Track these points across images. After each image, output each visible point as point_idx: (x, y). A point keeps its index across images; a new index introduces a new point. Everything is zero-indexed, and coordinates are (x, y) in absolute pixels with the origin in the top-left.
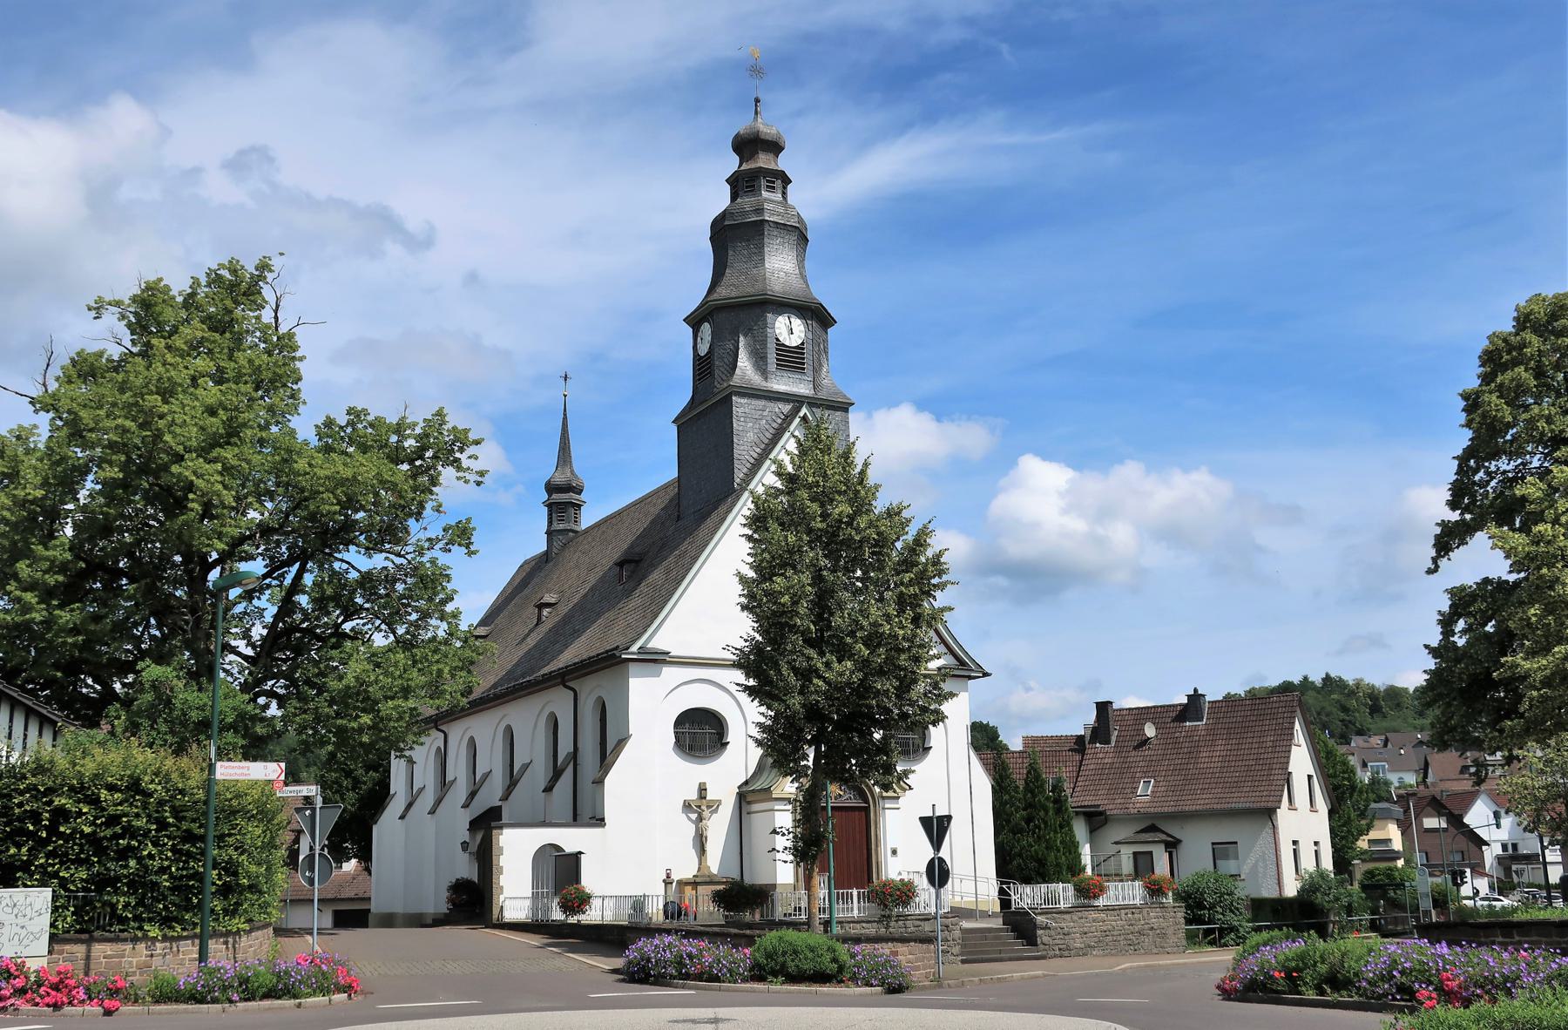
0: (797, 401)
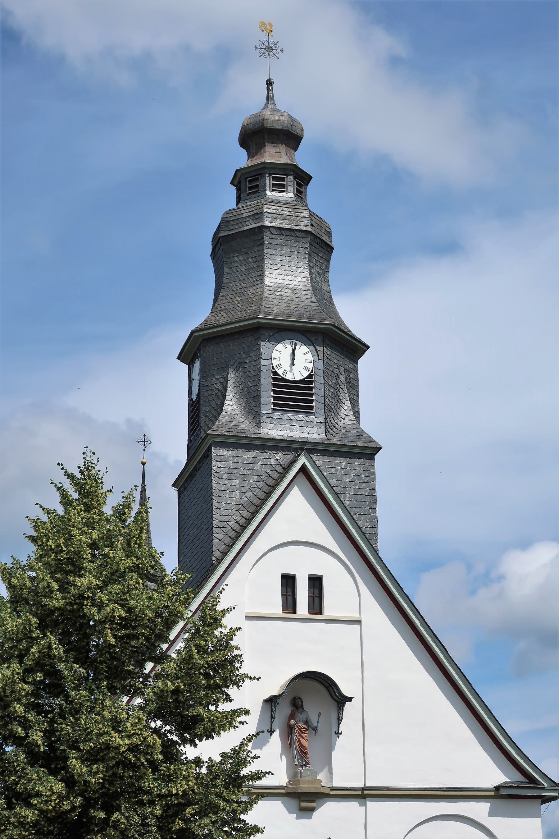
0: (294, 447)
